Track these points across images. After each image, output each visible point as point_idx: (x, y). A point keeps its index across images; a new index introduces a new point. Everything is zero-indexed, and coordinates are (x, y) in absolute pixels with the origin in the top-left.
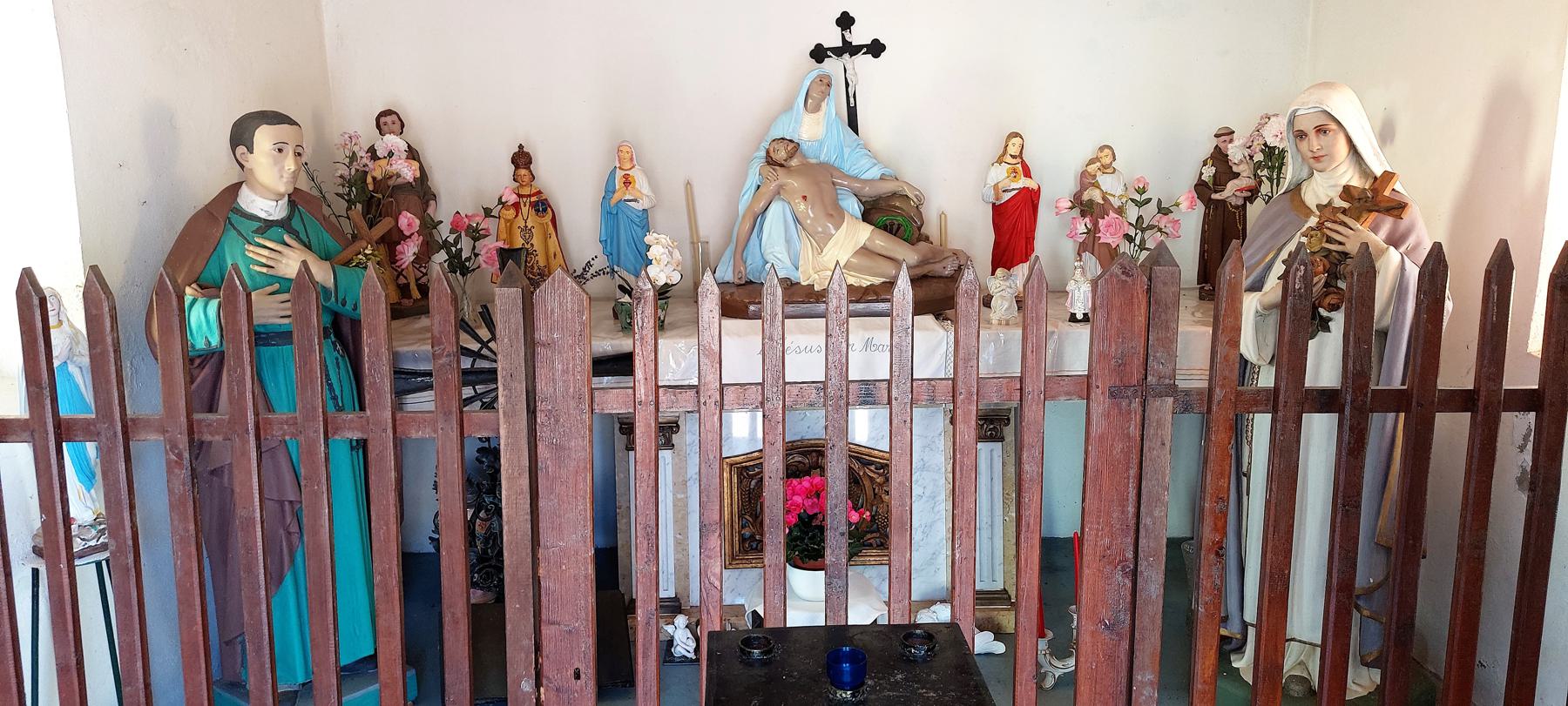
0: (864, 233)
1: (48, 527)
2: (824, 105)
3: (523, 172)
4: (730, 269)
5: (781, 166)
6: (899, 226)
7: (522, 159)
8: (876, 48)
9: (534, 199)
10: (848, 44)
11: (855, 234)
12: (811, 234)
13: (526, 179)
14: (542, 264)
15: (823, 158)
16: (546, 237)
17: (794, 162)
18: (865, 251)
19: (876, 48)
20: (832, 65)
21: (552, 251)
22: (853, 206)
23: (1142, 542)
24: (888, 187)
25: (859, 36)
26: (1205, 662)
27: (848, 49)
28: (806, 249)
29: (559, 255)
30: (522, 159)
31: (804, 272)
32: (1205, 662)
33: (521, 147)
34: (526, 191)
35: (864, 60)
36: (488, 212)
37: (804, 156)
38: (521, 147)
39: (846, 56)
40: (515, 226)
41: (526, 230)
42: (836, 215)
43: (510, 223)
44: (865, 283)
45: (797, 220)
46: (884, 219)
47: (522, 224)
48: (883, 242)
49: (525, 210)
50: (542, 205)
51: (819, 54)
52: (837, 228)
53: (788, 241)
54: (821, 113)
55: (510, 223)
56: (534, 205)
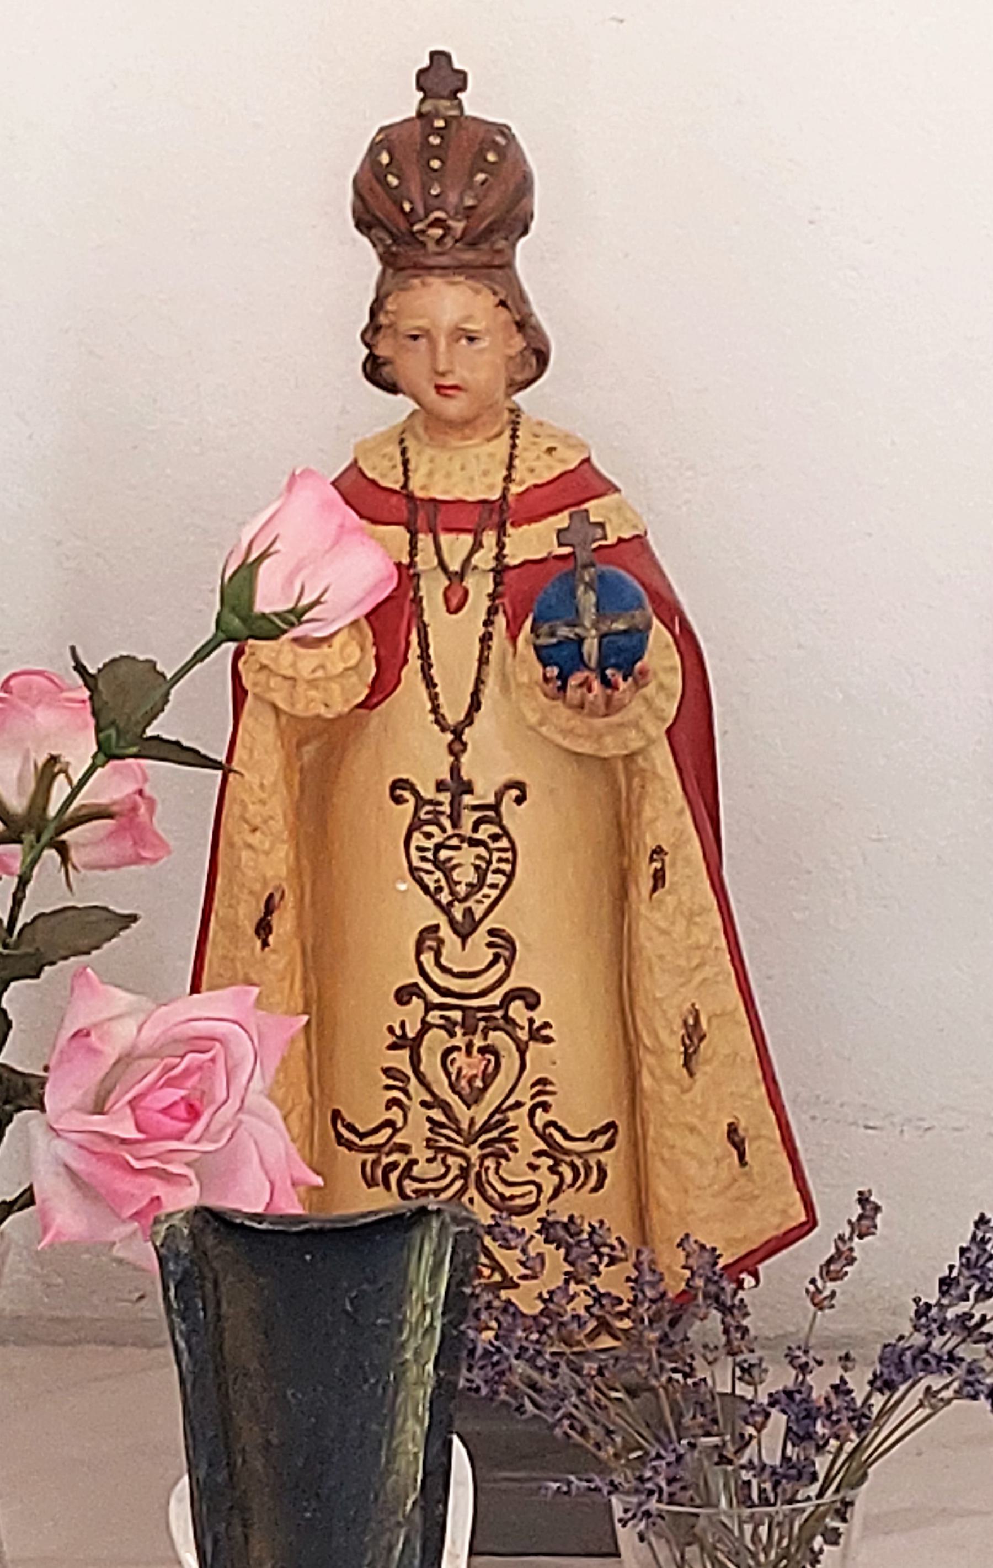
1: (477, 551)
3: (447, 302)
7: (440, 194)
9: (531, 542)
13: (480, 367)
14: (581, 1104)
16: (621, 875)
21: (664, 1003)
26: (770, 1343)
29: (728, 1040)
30: (440, 194)
32: (770, 1343)
33: (440, 78)
34: (460, 472)
36: (123, 706)
38: (440, 78)
40: (367, 773)
41: (456, 815)
43: (322, 752)
47: (427, 764)
49: (453, 637)
50: (595, 613)
55: (322, 752)
56: (527, 597)
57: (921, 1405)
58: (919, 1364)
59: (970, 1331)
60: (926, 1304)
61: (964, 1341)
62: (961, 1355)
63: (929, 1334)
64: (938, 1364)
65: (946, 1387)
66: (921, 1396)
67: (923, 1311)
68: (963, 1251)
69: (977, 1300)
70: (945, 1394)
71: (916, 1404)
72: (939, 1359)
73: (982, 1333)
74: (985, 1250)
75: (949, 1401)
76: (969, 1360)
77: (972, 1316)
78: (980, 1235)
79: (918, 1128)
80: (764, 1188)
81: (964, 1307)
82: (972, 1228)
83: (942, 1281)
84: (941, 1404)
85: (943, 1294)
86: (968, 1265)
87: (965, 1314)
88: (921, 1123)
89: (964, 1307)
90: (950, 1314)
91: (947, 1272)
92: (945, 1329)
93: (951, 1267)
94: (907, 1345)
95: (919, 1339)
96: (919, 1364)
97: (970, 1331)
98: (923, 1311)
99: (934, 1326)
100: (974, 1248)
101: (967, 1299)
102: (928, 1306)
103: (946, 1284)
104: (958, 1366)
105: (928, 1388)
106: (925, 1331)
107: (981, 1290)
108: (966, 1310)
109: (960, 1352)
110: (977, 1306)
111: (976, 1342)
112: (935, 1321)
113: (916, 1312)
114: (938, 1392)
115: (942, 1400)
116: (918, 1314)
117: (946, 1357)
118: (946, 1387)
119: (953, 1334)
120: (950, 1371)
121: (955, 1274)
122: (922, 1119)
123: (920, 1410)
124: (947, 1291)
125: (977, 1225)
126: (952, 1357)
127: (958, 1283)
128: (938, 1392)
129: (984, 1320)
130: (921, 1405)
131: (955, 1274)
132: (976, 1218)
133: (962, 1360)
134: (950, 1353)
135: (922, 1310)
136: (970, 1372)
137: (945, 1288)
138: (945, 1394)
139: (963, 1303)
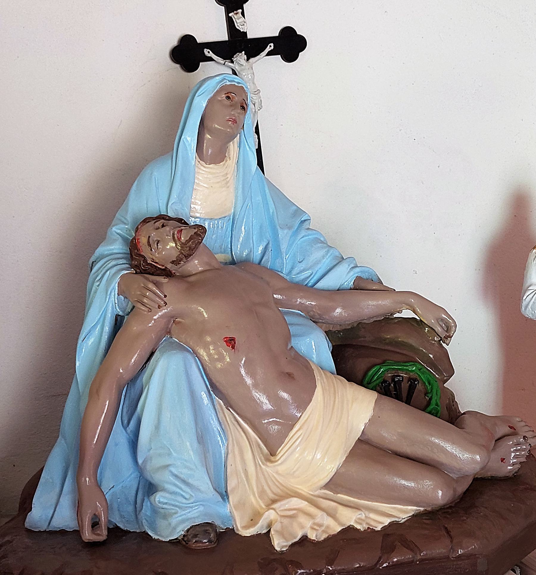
0: (356, 409)
2: (233, 147)
4: (66, 502)
5: (167, 273)
6: (413, 382)
8: (289, 45)
10: (231, 45)
11: (349, 411)
12: (253, 418)
15: (239, 251)
17: (195, 265)
18: (367, 449)
19: (289, 45)
20: (214, 72)
22: (316, 347)
23: (52, 513)
24: (371, 306)
25: (258, 22)
27: (238, 45)
28: (240, 446)
31: (241, 505)
35: (267, 68)
37: (210, 254)
39: (241, 57)
42: (296, 375)
44: (380, 522)
45: (214, 388)
46: (381, 371)
48: (402, 427)
51: (188, 53)
52: (303, 403)
53: (202, 438)
54: (231, 163)
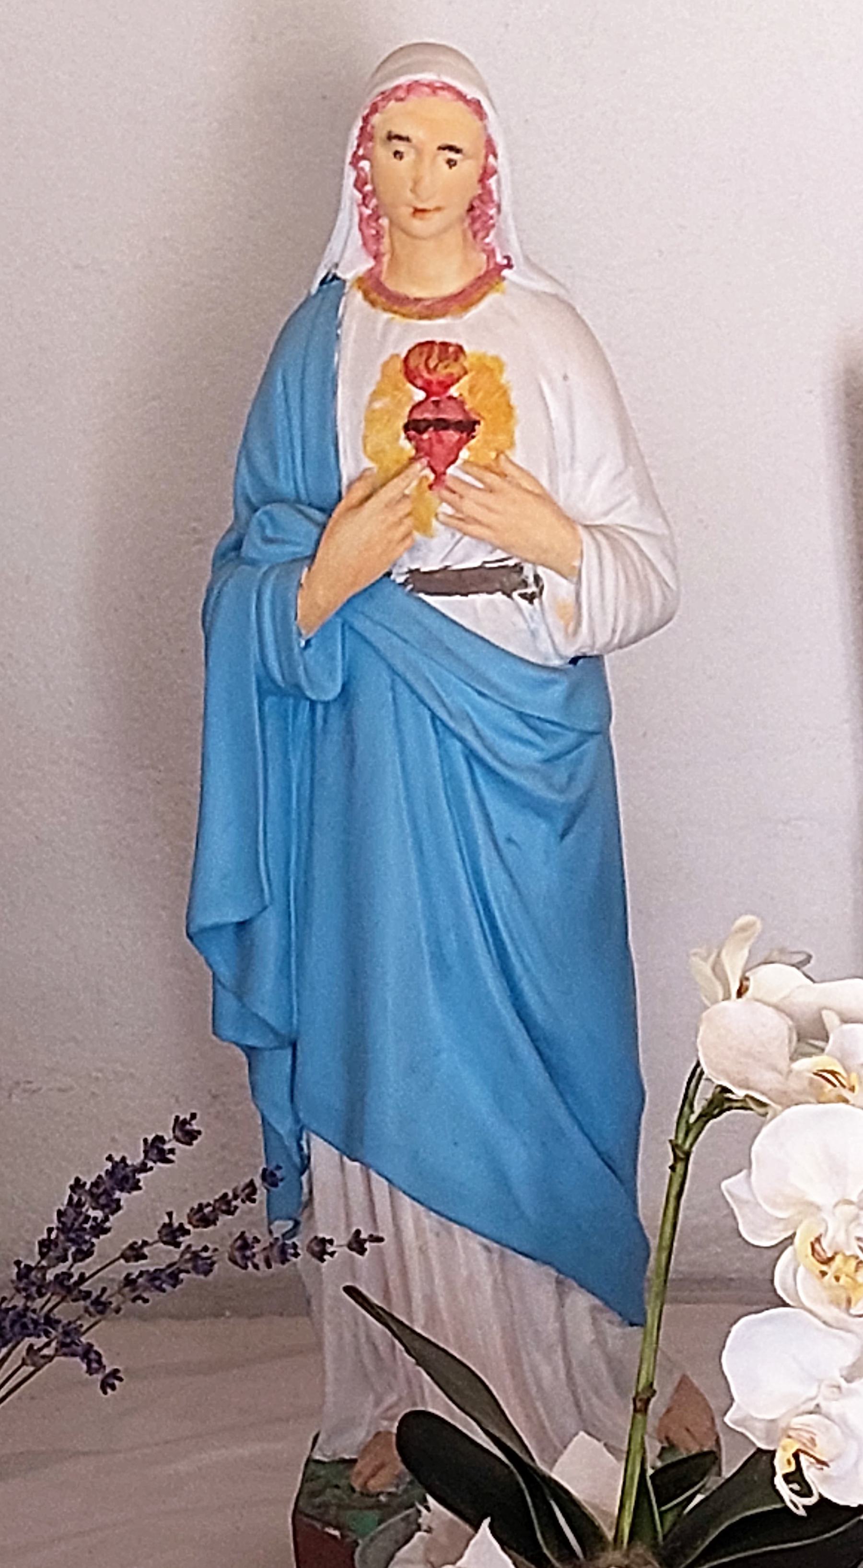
57: (24, 1363)
58: (17, 1328)
59: (69, 1290)
60: (26, 1266)
61: (63, 1299)
62: (57, 1317)
63: (28, 1297)
64: (35, 1328)
65: (47, 1345)
66: (24, 1353)
67: (25, 1273)
68: (60, 1214)
69: (75, 1261)
70: (46, 1352)
71: (20, 1362)
72: (35, 1322)
73: (80, 1291)
74: (81, 1213)
75: (50, 1358)
76: (65, 1322)
77: (71, 1276)
78: (76, 1198)
79: (25, 1091)
80: (117, 937)
81: (62, 1268)
82: (69, 1192)
83: (42, 1244)
84: (42, 1361)
85: (43, 1255)
86: (63, 1229)
87: (63, 1273)
88: (28, 1086)
89: (62, 1268)
90: (50, 1276)
91: (45, 1236)
92: (44, 1291)
93: (50, 1230)
94: (10, 1306)
95: (19, 1302)
96: (17, 1328)
97: (69, 1290)
98: (25, 1273)
99: (34, 1289)
100: (71, 1211)
101: (65, 1259)
102: (29, 1268)
103: (46, 1245)
104: (54, 1329)
105: (31, 1346)
106: (24, 1294)
107: (79, 1251)
108: (65, 1270)
109: (56, 1314)
110: (76, 1265)
111: (75, 1300)
112: (33, 1284)
113: (18, 1274)
114: (40, 1349)
115: (44, 1357)
116: (20, 1276)
117: (42, 1321)
118: (47, 1345)
119: (52, 1294)
120: (47, 1333)
121: (53, 1236)
122: (30, 1082)
123: (24, 1368)
124: (47, 1253)
125: (72, 1188)
126: (50, 1321)
127: (56, 1245)
128: (40, 1349)
129: (82, 1279)
130: (24, 1363)
131: (53, 1236)
132: (72, 1182)
133: (58, 1322)
134: (47, 1317)
135: (24, 1271)
136: (66, 1333)
137: (45, 1250)
138: (46, 1352)
139: (61, 1264)
